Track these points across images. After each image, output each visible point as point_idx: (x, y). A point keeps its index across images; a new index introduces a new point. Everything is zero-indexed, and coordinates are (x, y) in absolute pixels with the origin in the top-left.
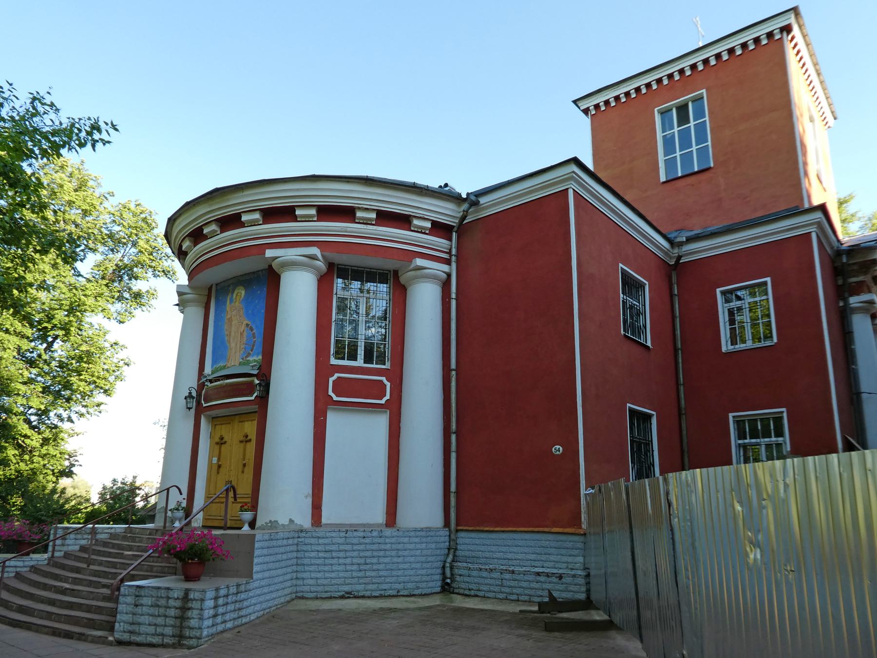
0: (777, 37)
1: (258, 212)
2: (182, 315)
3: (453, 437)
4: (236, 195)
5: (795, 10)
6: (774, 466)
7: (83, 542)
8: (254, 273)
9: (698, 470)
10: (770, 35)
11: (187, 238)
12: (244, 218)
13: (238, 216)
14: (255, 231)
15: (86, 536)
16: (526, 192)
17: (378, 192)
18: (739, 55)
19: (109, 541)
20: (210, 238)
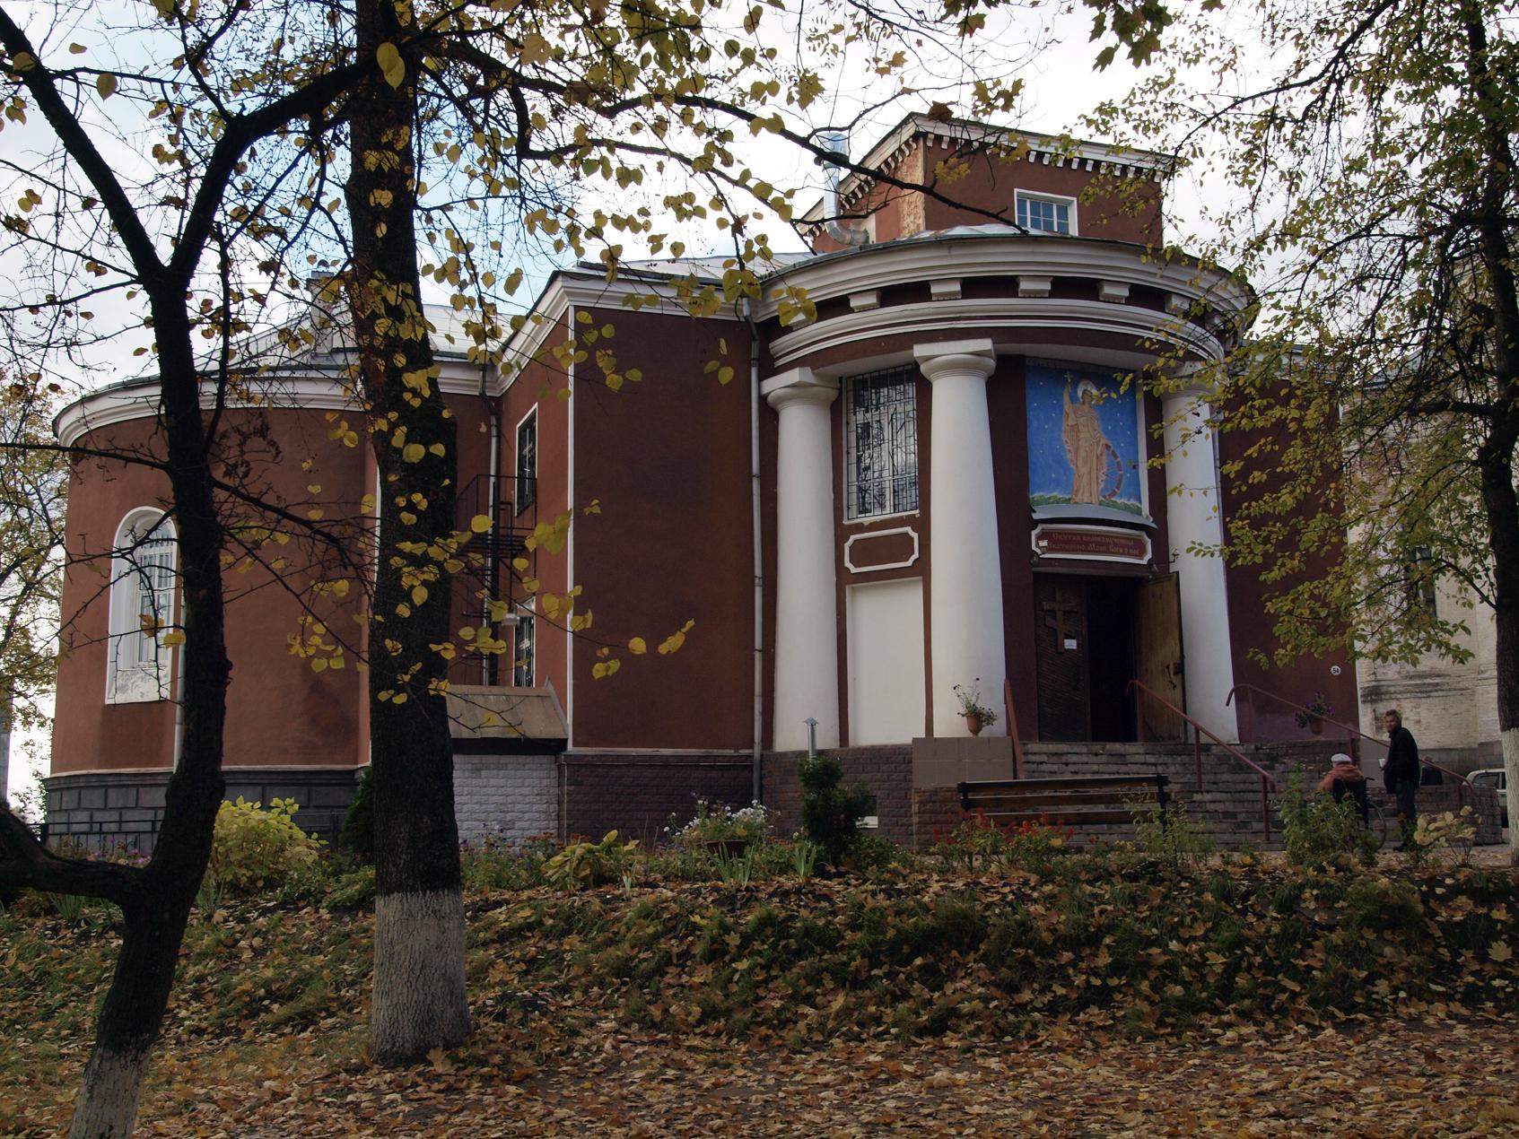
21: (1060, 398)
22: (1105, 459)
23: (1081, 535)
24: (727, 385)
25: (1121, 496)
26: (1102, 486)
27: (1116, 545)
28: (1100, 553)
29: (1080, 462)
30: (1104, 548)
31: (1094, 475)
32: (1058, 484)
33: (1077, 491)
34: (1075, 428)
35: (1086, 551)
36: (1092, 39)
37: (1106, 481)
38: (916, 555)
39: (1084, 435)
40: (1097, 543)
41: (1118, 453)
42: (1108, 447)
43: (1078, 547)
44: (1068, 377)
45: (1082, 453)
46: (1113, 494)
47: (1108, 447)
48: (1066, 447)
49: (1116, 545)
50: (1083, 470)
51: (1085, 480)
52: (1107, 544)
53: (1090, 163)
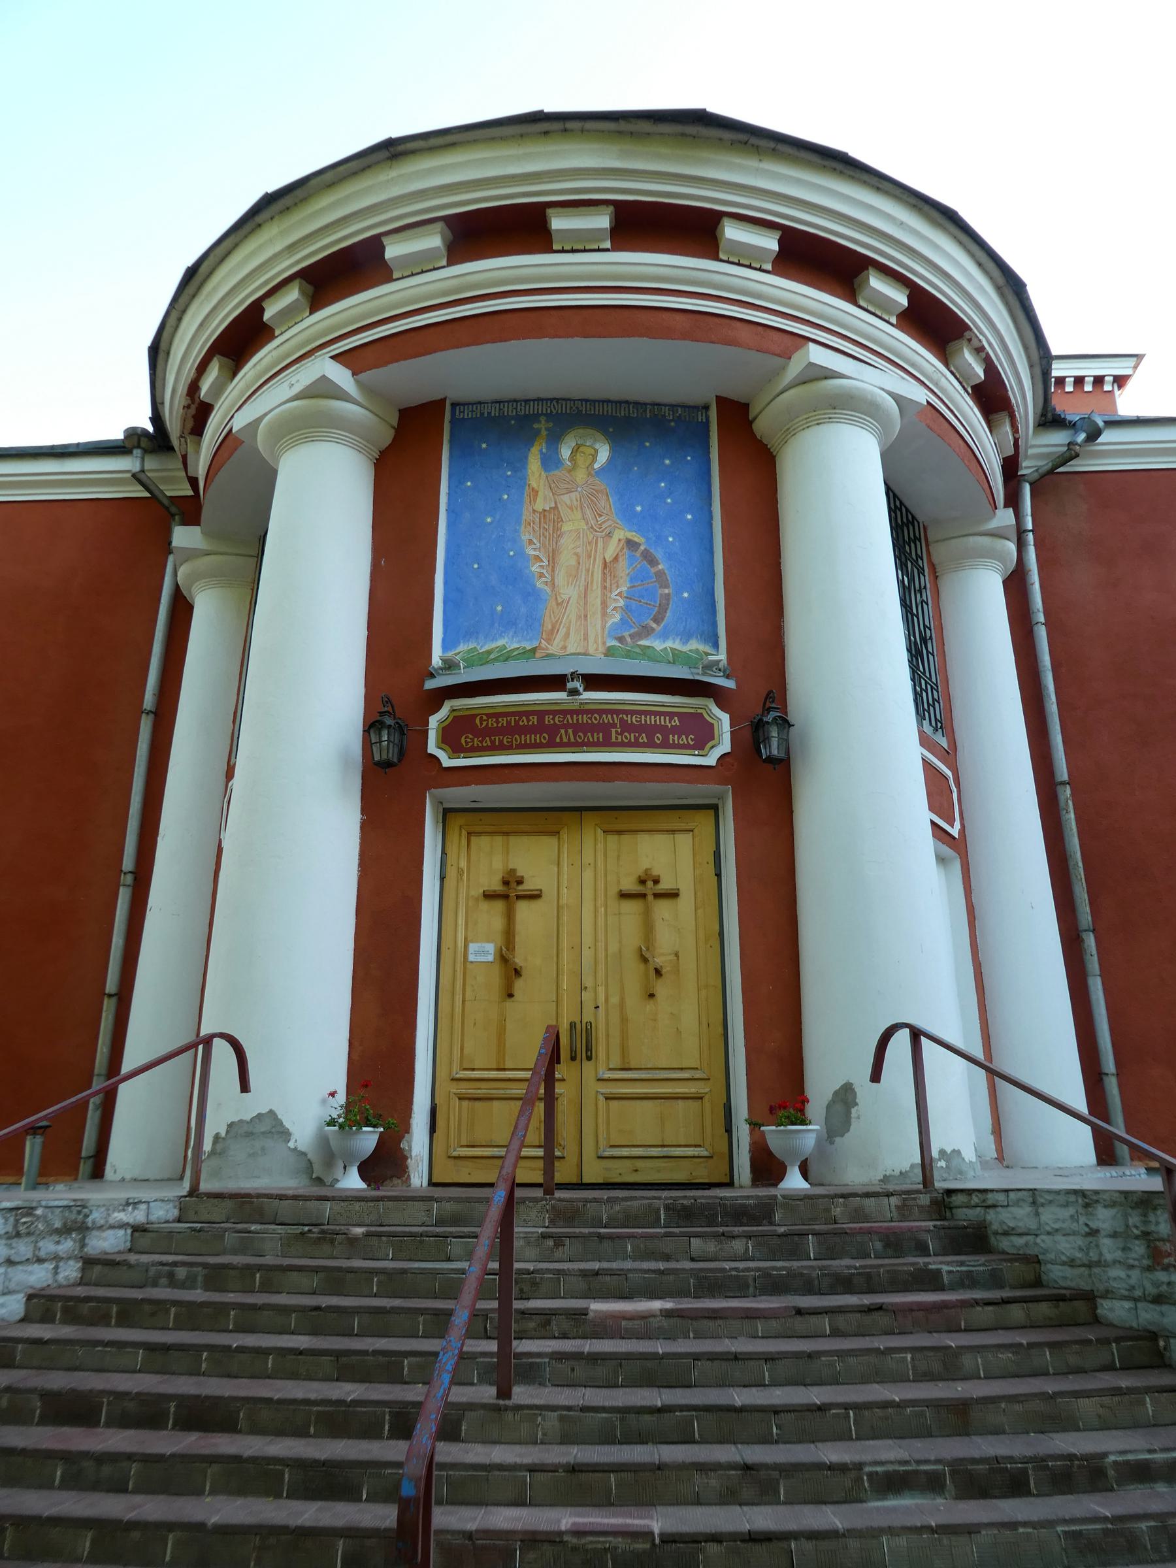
0: (1107, 387)
1: (777, 235)
2: (121, 436)
3: (111, 985)
4: (738, 160)
5: (1139, 357)
6: (526, 1237)
7: (38, 1276)
8: (637, 404)
9: (516, 1230)
10: (1099, 381)
11: (439, 226)
12: (393, 251)
13: (373, 248)
14: (385, 300)
15: (48, 1246)
16: (81, 480)
17: (194, 355)
18: (1106, 392)
19: (81, 1291)
20: (563, 251)
21: (520, 465)
22: (623, 569)
23: (541, 714)
24: (1045, 620)
25: (664, 636)
26: (617, 618)
27: (626, 727)
28: (635, 745)
29: (560, 579)
30: (644, 738)
31: (595, 599)
32: (509, 623)
33: (553, 631)
34: (551, 519)
35: (552, 745)
36: (1144, 355)
37: (627, 609)
38: (446, 762)
39: (573, 524)
40: (577, 728)
41: (659, 554)
42: (631, 544)
43: (531, 738)
44: (542, 425)
45: (566, 559)
46: (646, 631)
47: (631, 544)
48: (530, 551)
49: (626, 727)
50: (570, 592)
51: (572, 611)
52: (605, 729)
53: (1070, 381)
